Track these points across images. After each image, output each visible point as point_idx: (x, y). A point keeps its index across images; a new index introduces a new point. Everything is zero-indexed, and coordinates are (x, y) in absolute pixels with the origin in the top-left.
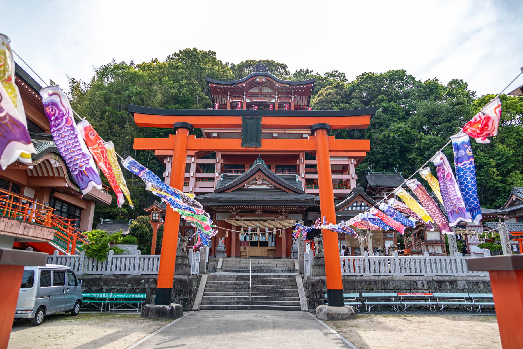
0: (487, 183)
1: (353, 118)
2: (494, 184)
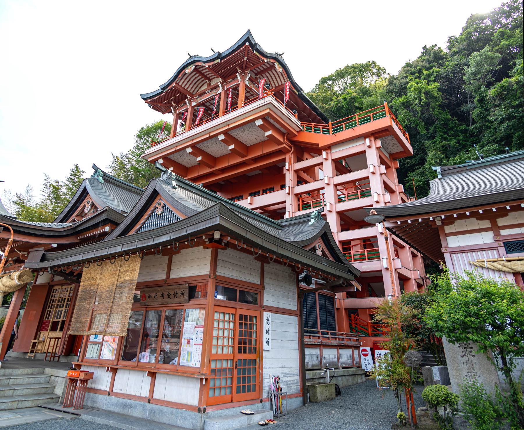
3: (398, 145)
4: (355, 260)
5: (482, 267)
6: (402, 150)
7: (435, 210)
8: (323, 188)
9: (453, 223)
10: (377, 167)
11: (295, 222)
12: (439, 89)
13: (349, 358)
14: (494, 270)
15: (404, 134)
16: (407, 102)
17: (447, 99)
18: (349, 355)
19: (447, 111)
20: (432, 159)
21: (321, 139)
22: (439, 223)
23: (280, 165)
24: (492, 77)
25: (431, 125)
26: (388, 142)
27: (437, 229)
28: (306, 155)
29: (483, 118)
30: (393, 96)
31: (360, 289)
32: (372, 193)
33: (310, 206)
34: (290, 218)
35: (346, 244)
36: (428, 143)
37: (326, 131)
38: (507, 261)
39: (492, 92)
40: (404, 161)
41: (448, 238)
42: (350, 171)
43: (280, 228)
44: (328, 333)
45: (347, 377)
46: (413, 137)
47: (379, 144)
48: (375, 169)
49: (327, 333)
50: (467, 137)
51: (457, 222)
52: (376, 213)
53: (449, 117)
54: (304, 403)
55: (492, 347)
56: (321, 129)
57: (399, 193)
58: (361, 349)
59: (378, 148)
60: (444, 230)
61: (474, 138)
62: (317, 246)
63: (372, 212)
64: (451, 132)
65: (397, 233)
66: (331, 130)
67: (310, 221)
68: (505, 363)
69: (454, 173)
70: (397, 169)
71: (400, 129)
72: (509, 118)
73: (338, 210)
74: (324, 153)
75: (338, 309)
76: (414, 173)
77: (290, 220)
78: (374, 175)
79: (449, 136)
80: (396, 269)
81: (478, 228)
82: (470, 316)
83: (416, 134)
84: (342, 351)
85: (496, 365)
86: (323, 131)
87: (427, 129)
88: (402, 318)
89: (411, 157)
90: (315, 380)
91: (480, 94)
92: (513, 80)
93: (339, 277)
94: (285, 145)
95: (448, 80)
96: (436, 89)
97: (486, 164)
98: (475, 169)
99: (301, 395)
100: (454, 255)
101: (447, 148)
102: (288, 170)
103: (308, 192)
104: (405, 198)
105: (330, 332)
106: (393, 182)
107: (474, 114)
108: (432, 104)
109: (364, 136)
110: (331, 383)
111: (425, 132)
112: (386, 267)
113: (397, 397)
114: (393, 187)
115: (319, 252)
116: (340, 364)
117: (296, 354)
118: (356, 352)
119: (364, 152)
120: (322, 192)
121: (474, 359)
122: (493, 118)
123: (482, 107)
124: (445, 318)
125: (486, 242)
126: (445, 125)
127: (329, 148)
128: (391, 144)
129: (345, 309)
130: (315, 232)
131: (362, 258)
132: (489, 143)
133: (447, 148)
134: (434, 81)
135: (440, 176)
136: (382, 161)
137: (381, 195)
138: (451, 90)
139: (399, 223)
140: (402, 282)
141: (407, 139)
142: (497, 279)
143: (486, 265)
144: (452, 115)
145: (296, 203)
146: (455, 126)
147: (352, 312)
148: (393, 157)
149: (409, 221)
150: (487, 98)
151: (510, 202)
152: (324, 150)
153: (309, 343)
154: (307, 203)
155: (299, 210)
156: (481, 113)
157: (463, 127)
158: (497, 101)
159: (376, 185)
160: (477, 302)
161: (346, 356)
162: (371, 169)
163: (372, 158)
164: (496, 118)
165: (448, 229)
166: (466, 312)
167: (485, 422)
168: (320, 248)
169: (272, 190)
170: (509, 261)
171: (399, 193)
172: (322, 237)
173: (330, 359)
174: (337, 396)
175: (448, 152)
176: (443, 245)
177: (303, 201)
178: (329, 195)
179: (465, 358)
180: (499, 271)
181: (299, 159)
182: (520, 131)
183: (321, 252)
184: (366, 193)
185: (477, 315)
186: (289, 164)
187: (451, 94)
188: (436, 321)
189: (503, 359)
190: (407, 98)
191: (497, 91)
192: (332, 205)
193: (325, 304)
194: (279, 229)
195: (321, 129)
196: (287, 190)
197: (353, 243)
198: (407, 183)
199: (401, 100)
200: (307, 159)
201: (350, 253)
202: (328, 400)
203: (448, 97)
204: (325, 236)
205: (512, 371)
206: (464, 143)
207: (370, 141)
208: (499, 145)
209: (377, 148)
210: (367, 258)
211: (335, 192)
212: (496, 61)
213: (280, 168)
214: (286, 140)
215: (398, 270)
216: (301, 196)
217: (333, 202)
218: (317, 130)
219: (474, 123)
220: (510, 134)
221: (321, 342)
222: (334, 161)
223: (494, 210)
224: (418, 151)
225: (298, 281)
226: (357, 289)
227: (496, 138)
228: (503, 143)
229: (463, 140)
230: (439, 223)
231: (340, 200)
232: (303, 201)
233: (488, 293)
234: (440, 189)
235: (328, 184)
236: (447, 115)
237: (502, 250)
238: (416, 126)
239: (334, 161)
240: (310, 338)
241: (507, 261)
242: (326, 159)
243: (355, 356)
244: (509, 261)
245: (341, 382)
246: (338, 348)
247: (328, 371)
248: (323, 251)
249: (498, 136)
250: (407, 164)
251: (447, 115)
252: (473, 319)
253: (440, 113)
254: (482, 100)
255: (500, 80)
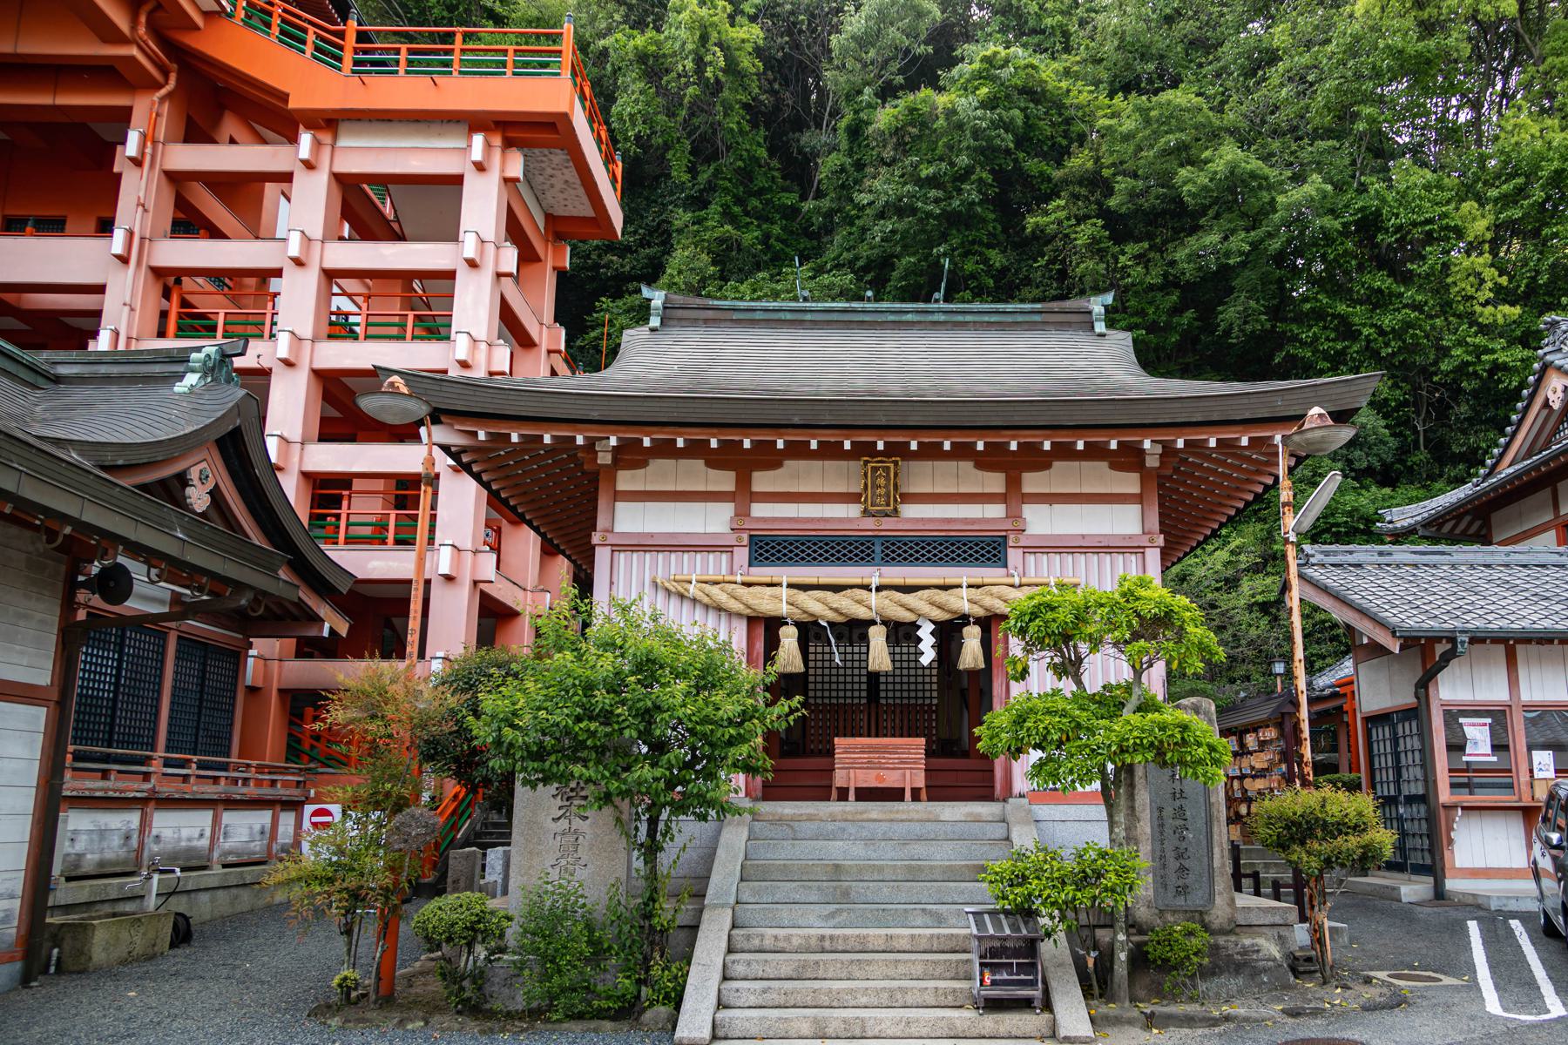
0: (1444, 352)
1: (250, 519)
2: (1479, 351)
3: (581, 191)
4: (349, 541)
5: (682, 596)
6: (590, 213)
7: (595, 415)
8: (278, 273)
9: (642, 464)
10: (490, 248)
11: (115, 370)
12: (758, 52)
13: (258, 837)
14: (707, 607)
15: (608, 160)
16: (656, 57)
17: (773, 92)
18: (257, 828)
19: (762, 132)
20: (680, 272)
21: (307, 81)
22: (605, 459)
23: (105, 131)
24: (901, 71)
25: (708, 161)
26: (549, 171)
27: (597, 474)
28: (230, 126)
29: (843, 186)
30: (617, 17)
31: (343, 629)
32: (454, 328)
33: (213, 329)
34: (114, 352)
35: (329, 490)
36: (682, 217)
37: (329, 53)
38: (744, 584)
39: (885, 117)
40: (600, 256)
41: (619, 505)
42: (400, 237)
43: (41, 381)
44: (190, 761)
45: (234, 891)
46: (640, 180)
47: (516, 168)
48: (482, 253)
49: (183, 764)
50: (792, 232)
51: (656, 464)
52: (405, 390)
53: (762, 153)
54: (26, 980)
55: (626, 794)
56: (311, 38)
57: (549, 352)
58: (309, 809)
59: (508, 182)
60: (614, 481)
61: (806, 241)
62: (194, 474)
63: (392, 384)
64: (755, 203)
65: (475, 469)
66: (348, 57)
67: (181, 377)
68: (652, 832)
69: (694, 322)
70: (561, 274)
71: (599, 141)
72: (898, 209)
73: (318, 365)
74: (306, 139)
75: (253, 690)
76: (620, 303)
77: (113, 357)
78: (474, 272)
79: (747, 214)
80: (475, 583)
81: (701, 488)
82: (591, 719)
83: (657, 178)
84: (228, 817)
85: (630, 836)
86: (317, 49)
87: (693, 171)
88: (411, 719)
89: (612, 247)
90: (98, 907)
91: (856, 112)
92: (942, 100)
93: (239, 586)
94: (134, 51)
95: (790, 33)
96: (749, 47)
97: (782, 316)
98: (753, 323)
99: (19, 955)
100: (622, 555)
101: (729, 249)
102: (137, 162)
103: (217, 276)
104: (562, 368)
105: (195, 759)
106: (537, 314)
107: (828, 165)
108: (726, 94)
109: (475, 122)
110: (161, 911)
111: (685, 177)
112: (446, 571)
113: (348, 932)
114: (533, 330)
115: (198, 498)
116: (216, 855)
117: (20, 830)
118: (287, 820)
119: (458, 180)
120: (274, 281)
121: (583, 826)
122: (864, 198)
123: (850, 153)
124: (526, 720)
125: (710, 530)
126: (746, 175)
127: (329, 122)
128: (559, 185)
129: (280, 691)
130: (189, 422)
131: (376, 538)
132: (838, 267)
133: (729, 249)
134: (753, 19)
135: (655, 322)
136: (514, 230)
137: (483, 346)
138: (790, 68)
139: (482, 436)
140: (490, 621)
141: (614, 180)
142: (689, 624)
143: (693, 590)
144: (772, 152)
145: (155, 302)
146: (770, 189)
147: (303, 703)
148: (559, 228)
149: (515, 438)
150: (870, 129)
151: (790, 431)
152: (308, 127)
153: (98, 794)
154: (203, 316)
155: (162, 334)
156: (843, 170)
157: (789, 199)
158: (889, 147)
159: (473, 308)
160: (616, 685)
161: (245, 831)
162: (469, 248)
163: (481, 209)
164: (870, 197)
165: (626, 480)
166: (583, 706)
167: (559, 971)
168: (204, 484)
169: (52, 226)
170: (749, 585)
171: (549, 352)
172: (221, 443)
173: (180, 839)
174: (173, 945)
175: (730, 264)
176: (602, 522)
177: (185, 303)
178: (297, 302)
179: (563, 824)
180: (720, 609)
181: (197, 132)
182: (914, 254)
183: (207, 500)
184: (435, 329)
185: (607, 717)
186: (144, 137)
187: (786, 83)
188: (500, 729)
189: (653, 823)
190: (658, 44)
191: (896, 118)
192: (294, 345)
193: (204, 672)
194: (35, 387)
195: (311, 38)
196: (118, 242)
197: (357, 485)
198: (593, 328)
199: (640, 41)
200: (232, 141)
201: (338, 517)
202: (137, 960)
203: (776, 86)
204: (238, 445)
205: (662, 849)
206: (778, 246)
207: (488, 146)
208: (859, 279)
209: (507, 181)
210: (391, 536)
211: (325, 295)
212: (924, 26)
213: (108, 143)
214: (142, 30)
215: (482, 586)
216: (178, 282)
217: (306, 331)
218: (292, 37)
219: (820, 195)
220: (893, 256)
221: (153, 790)
222: (339, 179)
223: (747, 444)
224: (651, 234)
225: (71, 587)
226: (332, 630)
227: (857, 258)
228: (868, 277)
229: (778, 239)
230: (605, 459)
231: (339, 329)
232: (185, 303)
233: (654, 662)
234: (640, 359)
235: (298, 262)
236: (759, 145)
237: (742, 555)
238: (667, 146)
239: (339, 179)
240: (105, 775)
241: (744, 584)
242: (309, 165)
243: (281, 829)
244: (749, 585)
245: (202, 909)
246: (278, 808)
247: (156, 877)
248: (215, 494)
249: (864, 251)
250: (607, 266)
251: (759, 145)
252: (593, 726)
253: (741, 131)
254: (855, 131)
255: (912, 86)
